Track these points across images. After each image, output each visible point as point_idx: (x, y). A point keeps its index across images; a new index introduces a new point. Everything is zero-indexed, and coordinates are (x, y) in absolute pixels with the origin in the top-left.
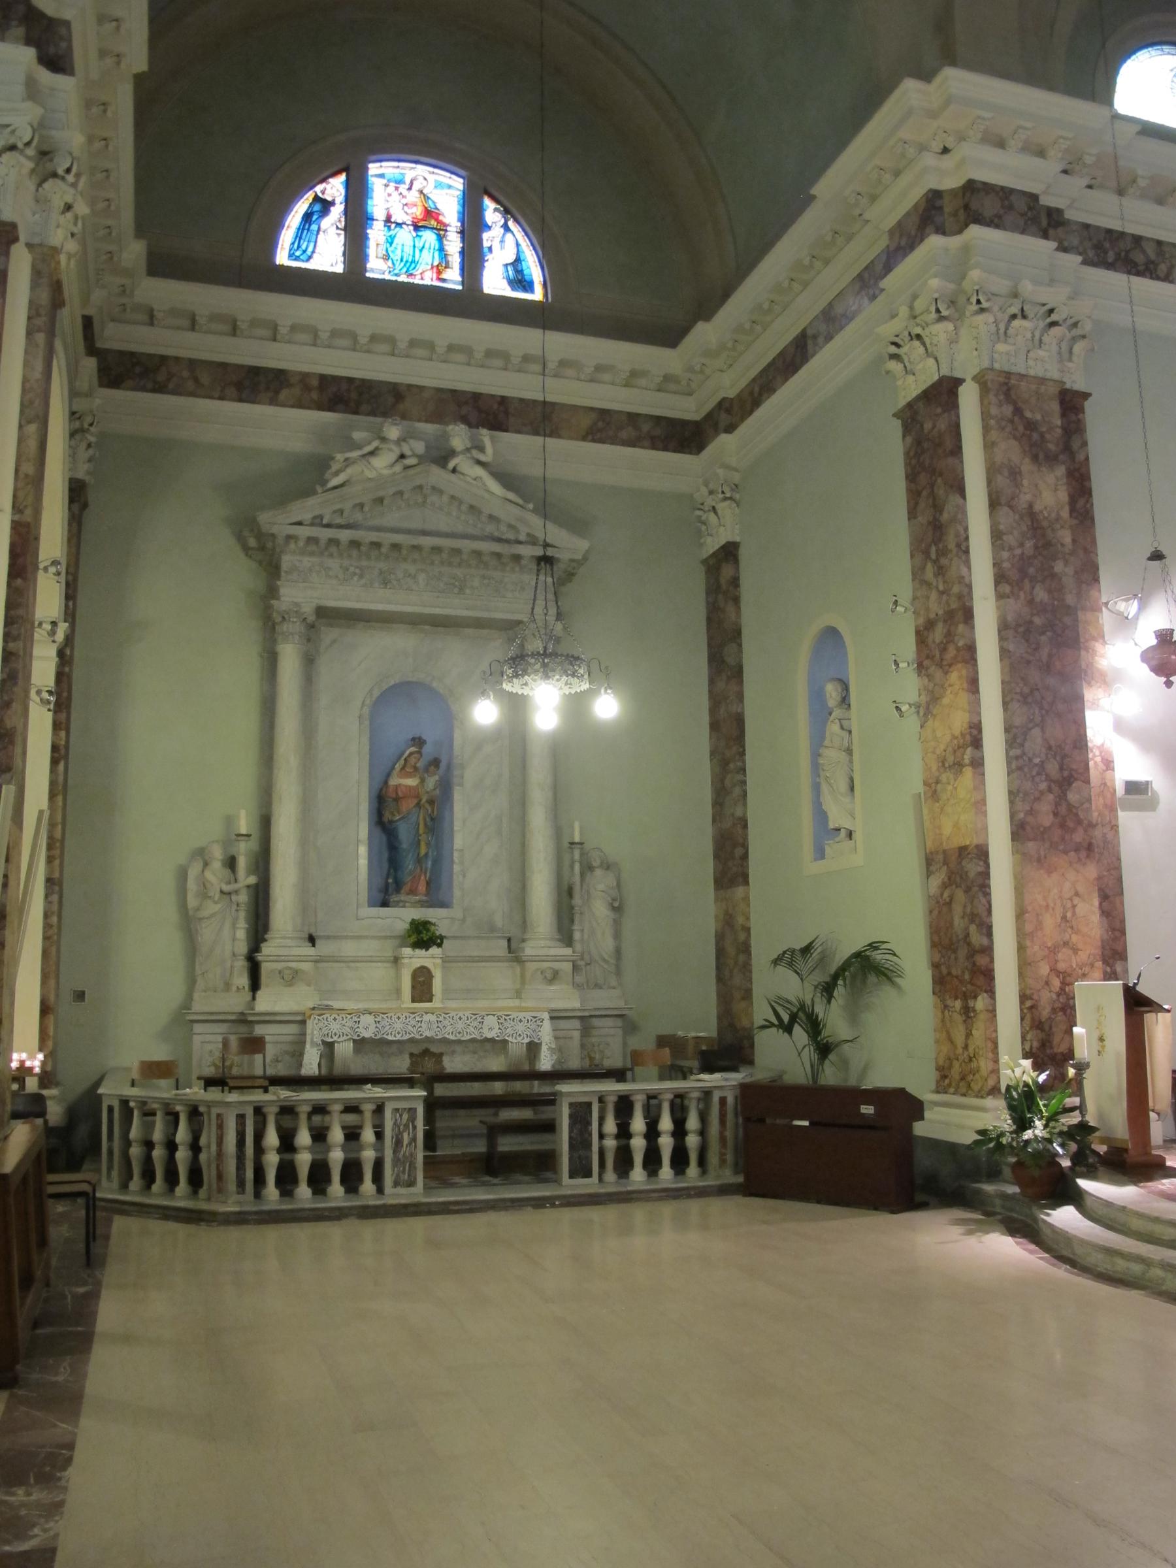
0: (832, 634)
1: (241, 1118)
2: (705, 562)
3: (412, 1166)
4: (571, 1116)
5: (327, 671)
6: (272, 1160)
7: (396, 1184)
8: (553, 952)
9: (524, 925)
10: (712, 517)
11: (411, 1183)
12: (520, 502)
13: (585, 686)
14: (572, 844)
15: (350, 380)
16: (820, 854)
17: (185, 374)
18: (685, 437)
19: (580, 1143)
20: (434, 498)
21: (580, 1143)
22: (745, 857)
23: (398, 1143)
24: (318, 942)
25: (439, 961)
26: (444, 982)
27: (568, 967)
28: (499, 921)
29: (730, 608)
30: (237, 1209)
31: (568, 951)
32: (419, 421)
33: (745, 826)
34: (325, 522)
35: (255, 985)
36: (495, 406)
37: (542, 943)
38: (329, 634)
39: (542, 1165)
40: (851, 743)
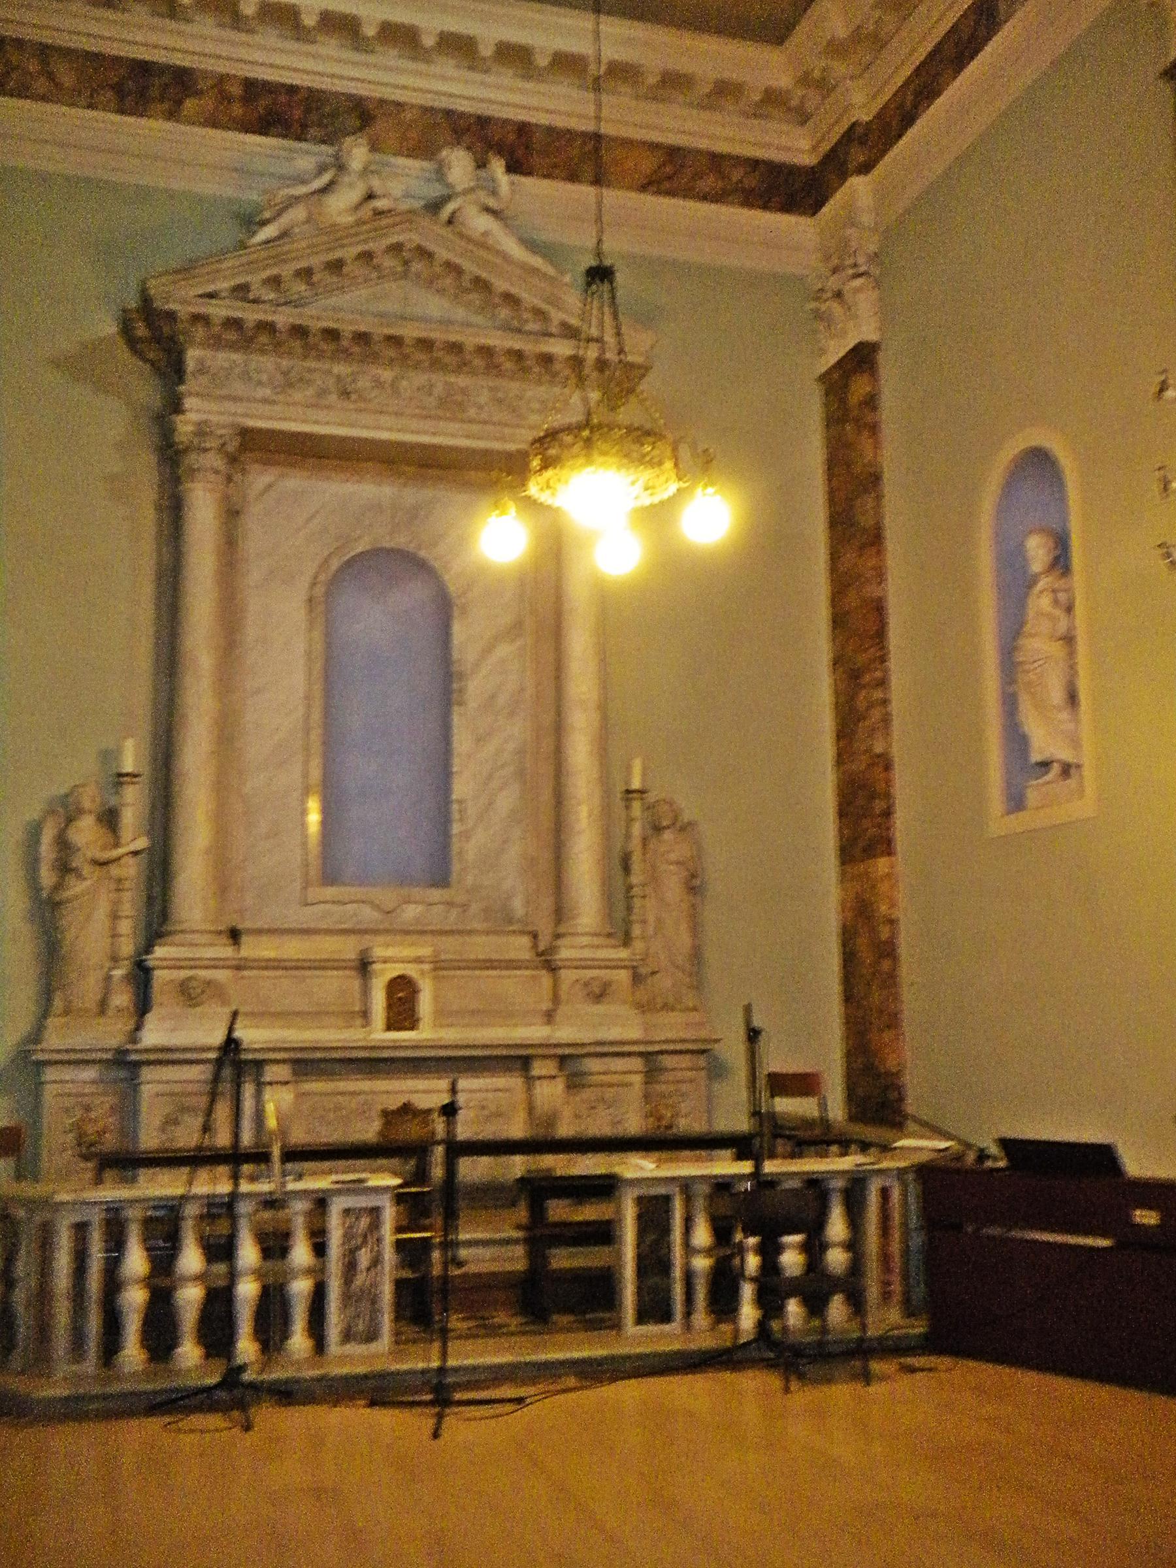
0: (1039, 461)
1: (81, 1229)
2: (823, 378)
3: (375, 1311)
4: (640, 1217)
5: (256, 536)
6: (135, 1298)
7: (348, 1336)
8: (602, 954)
9: (560, 913)
10: (836, 308)
11: (371, 1336)
12: (551, 271)
13: (673, 487)
14: (628, 792)
15: (292, 90)
16: (1016, 803)
17: (33, 66)
18: (794, 190)
19: (654, 1262)
20: (416, 266)
21: (654, 1262)
22: (888, 813)
23: (350, 1267)
24: (244, 939)
25: (427, 967)
26: (436, 998)
27: (623, 976)
28: (518, 906)
29: (866, 443)
30: (66, 1393)
31: (623, 954)
32: (398, 153)
33: (888, 767)
34: (251, 296)
35: (143, 1006)
36: (512, 137)
37: (585, 940)
38: (260, 478)
39: (593, 1297)
40: (1071, 628)
